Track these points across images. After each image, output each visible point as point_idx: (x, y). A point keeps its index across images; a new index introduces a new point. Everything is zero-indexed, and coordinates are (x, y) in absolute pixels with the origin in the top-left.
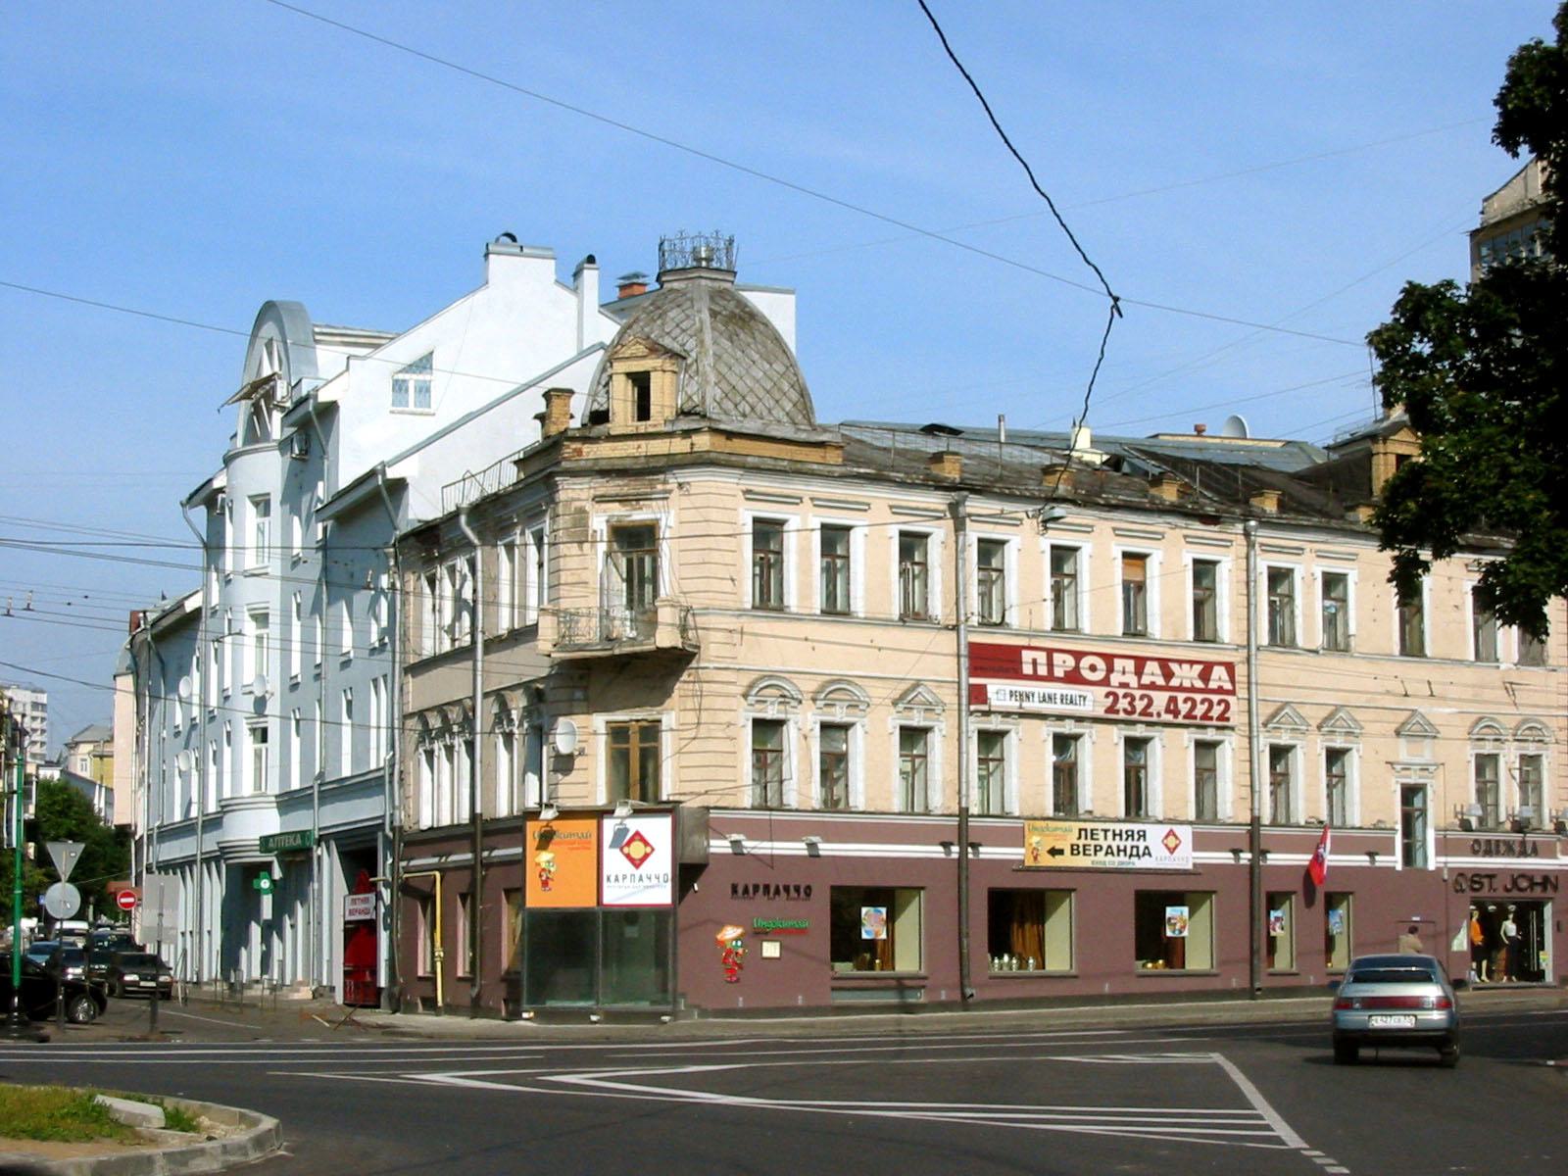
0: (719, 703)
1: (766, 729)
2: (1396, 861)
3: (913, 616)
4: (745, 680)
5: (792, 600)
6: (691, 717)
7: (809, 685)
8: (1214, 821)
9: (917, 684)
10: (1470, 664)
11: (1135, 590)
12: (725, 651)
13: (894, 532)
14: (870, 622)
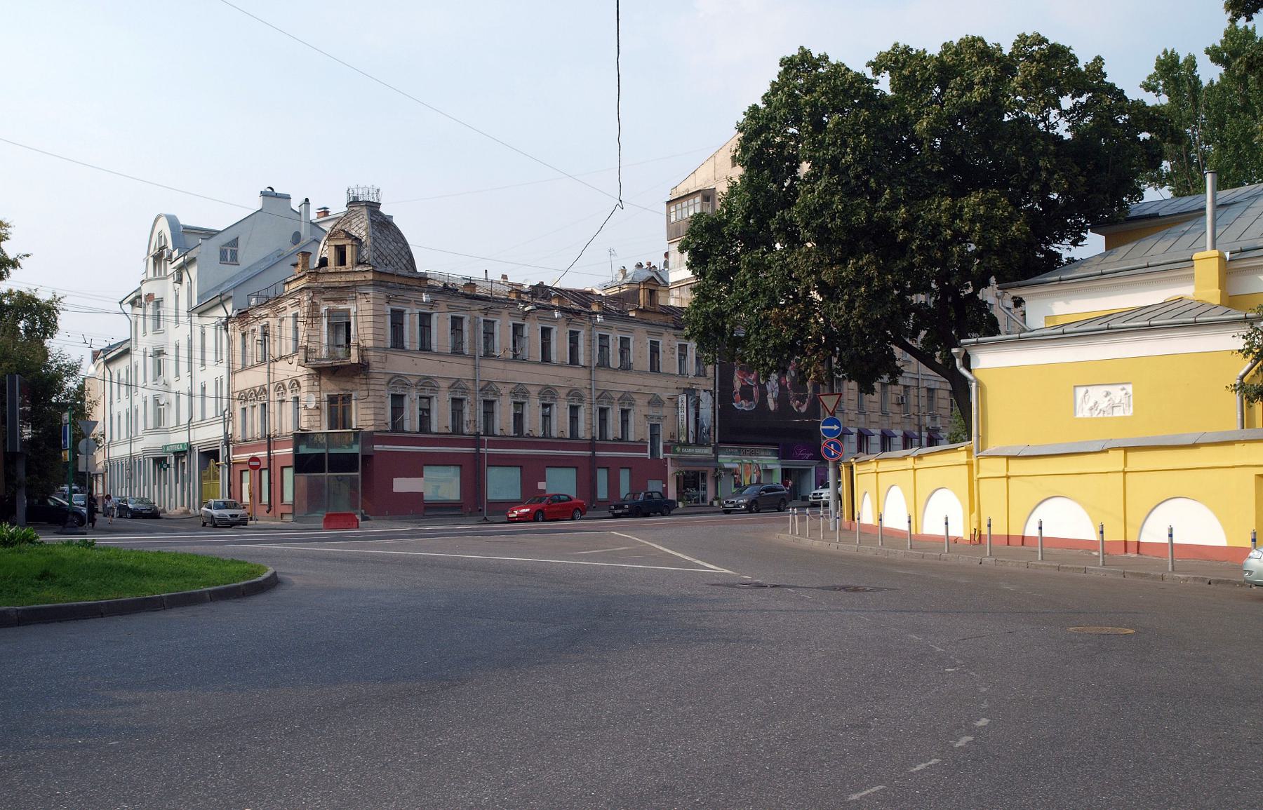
0: (377, 387)
1: (603, 412)
2: (648, 455)
3: (457, 351)
4: (388, 378)
5: (407, 345)
6: (366, 393)
7: (414, 381)
8: (577, 438)
9: (458, 380)
10: (538, 363)
11: (489, 335)
12: (380, 365)
13: (449, 315)
14: (438, 354)
